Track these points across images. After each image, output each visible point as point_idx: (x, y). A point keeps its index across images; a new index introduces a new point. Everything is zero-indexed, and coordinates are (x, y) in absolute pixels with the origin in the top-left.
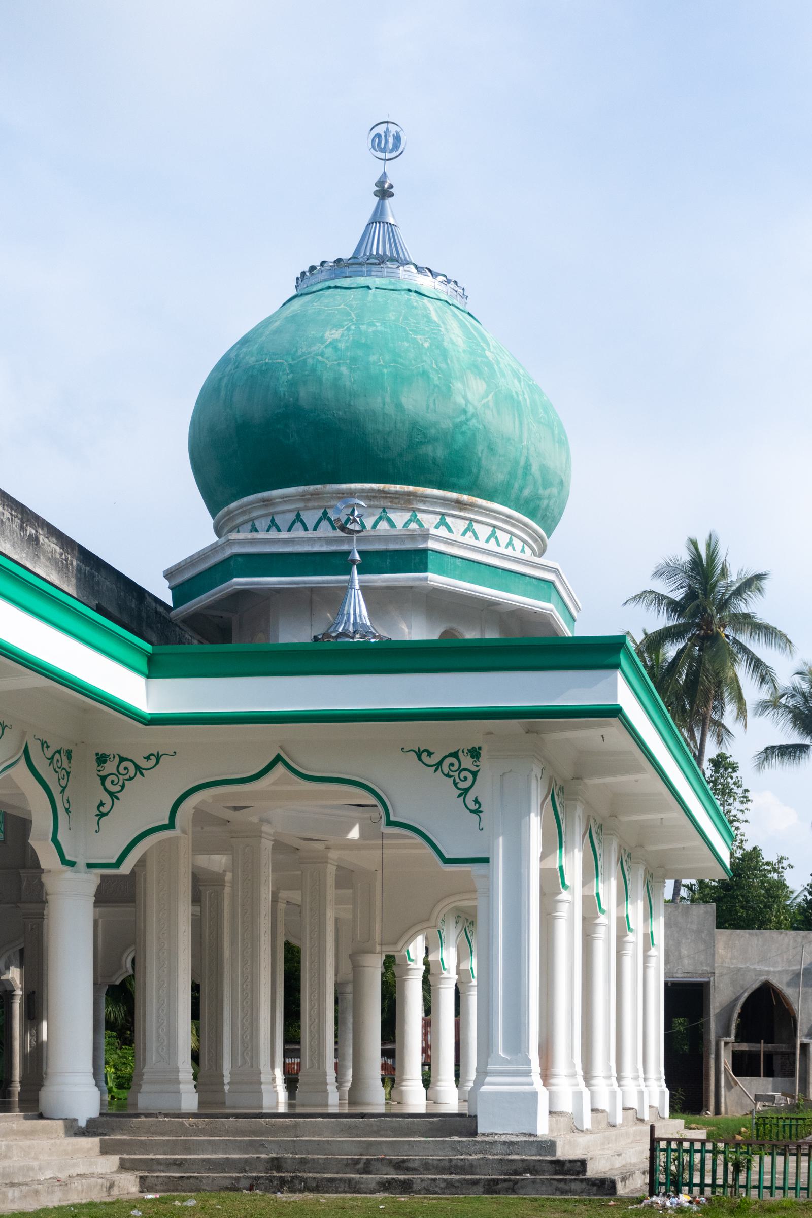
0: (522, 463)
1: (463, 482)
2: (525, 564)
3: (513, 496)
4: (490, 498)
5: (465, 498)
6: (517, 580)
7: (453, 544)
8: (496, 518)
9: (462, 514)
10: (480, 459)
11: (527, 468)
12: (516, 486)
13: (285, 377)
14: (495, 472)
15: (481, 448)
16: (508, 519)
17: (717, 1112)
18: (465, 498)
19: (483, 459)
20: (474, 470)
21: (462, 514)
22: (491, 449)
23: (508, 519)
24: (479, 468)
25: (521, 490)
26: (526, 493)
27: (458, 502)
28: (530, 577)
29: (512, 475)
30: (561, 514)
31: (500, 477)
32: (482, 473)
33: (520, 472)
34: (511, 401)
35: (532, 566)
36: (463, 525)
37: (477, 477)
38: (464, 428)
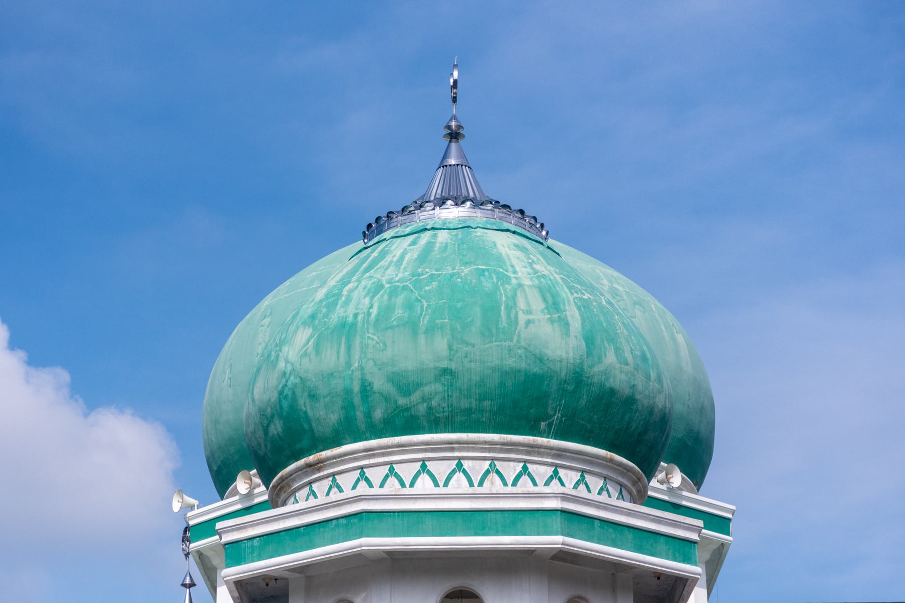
0: (356, 388)
1: (305, 443)
2: (327, 508)
3: (363, 427)
4: (339, 444)
5: (311, 458)
6: (322, 530)
7: (245, 528)
8: (356, 459)
9: (321, 474)
10: (306, 413)
11: (366, 390)
12: (359, 415)
13: (245, 445)
14: (327, 416)
15: (303, 401)
16: (370, 452)
17: (699, 575)
18: (311, 458)
19: (309, 411)
20: (306, 426)
21: (321, 474)
22: (313, 397)
23: (370, 452)
24: (309, 421)
25: (368, 415)
26: (378, 414)
27: (309, 465)
28: (337, 518)
29: (348, 407)
30: (712, 424)
31: (334, 418)
32: (314, 425)
33: (357, 400)
34: (347, 330)
35: (334, 506)
36: (327, 483)
37: (312, 430)
38: (286, 391)
